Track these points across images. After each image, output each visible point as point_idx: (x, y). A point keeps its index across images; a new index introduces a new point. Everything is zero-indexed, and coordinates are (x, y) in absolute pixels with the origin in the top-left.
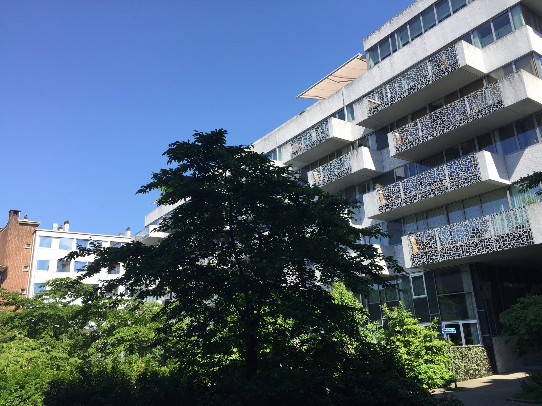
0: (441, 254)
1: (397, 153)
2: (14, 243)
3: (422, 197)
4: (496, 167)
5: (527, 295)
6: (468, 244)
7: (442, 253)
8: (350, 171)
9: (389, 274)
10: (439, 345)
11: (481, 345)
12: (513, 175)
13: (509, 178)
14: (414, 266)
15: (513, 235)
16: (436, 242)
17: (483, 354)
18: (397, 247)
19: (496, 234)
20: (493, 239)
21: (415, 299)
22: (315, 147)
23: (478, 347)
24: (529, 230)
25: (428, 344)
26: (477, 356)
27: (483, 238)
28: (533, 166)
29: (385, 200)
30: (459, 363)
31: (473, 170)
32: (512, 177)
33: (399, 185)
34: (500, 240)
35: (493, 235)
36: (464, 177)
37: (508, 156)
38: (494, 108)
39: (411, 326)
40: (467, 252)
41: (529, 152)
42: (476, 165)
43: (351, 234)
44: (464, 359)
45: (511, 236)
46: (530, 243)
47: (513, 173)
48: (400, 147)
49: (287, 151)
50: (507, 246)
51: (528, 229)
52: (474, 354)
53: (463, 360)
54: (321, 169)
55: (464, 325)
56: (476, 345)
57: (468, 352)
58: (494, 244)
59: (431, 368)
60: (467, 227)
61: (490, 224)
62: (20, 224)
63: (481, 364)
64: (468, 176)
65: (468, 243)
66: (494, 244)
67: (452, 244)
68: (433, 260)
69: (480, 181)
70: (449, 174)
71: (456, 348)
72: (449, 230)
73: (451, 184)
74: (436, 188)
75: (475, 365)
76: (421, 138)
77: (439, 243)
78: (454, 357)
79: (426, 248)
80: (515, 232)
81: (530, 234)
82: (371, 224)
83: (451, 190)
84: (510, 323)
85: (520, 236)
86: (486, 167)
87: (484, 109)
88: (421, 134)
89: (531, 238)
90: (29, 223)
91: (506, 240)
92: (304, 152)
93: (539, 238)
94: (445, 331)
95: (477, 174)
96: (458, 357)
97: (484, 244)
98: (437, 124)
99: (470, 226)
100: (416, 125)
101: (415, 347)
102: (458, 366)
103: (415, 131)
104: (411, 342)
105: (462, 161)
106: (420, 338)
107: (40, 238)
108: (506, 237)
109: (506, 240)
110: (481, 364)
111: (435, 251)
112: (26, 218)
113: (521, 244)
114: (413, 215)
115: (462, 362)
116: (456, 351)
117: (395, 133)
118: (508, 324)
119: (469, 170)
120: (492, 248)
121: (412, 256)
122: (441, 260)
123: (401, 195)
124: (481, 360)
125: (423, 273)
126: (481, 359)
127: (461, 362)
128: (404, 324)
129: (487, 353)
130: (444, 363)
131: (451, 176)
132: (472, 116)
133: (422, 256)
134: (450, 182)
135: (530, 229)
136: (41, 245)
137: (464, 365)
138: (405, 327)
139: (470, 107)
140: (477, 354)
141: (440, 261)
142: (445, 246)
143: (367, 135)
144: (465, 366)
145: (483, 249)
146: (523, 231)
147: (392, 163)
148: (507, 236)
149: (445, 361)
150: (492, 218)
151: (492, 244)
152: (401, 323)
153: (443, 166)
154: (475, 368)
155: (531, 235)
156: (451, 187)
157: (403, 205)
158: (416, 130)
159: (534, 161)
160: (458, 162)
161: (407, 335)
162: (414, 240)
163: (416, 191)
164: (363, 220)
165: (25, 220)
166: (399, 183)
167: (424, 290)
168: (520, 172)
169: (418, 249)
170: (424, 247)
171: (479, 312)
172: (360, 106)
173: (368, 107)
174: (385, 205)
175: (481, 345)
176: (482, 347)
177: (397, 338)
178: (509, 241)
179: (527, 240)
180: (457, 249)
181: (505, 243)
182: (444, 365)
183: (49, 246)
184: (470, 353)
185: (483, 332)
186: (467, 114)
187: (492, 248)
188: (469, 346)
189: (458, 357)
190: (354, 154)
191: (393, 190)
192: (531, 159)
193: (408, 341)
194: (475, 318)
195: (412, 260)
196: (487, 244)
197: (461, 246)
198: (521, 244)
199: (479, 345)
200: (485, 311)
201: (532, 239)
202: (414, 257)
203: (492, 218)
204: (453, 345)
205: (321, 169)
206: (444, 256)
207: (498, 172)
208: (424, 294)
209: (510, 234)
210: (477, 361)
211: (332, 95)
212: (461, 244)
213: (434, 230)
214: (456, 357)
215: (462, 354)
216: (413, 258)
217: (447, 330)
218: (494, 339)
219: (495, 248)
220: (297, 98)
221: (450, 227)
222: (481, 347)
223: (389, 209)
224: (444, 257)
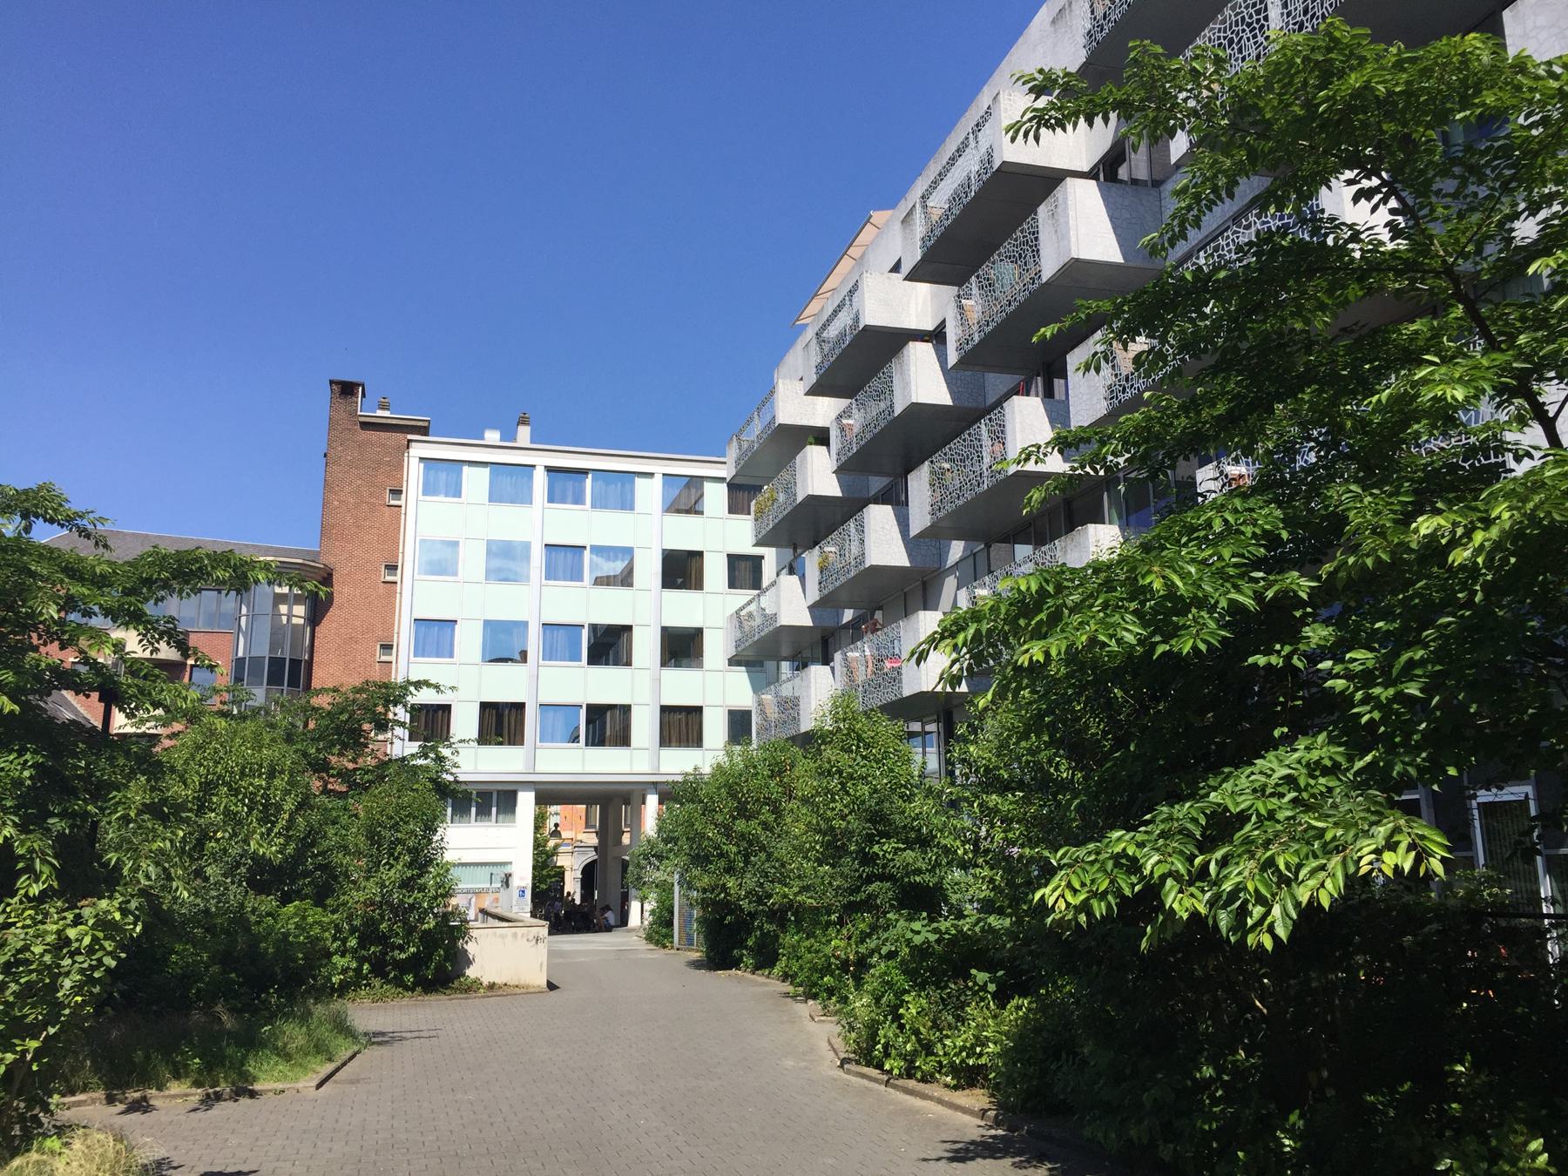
2: (348, 489)
9: (907, 564)
43: (1459, 165)
62: (366, 426)
90: (394, 422)
107: (422, 465)
112: (383, 407)
136: (429, 489)
165: (380, 413)
183: (627, 504)
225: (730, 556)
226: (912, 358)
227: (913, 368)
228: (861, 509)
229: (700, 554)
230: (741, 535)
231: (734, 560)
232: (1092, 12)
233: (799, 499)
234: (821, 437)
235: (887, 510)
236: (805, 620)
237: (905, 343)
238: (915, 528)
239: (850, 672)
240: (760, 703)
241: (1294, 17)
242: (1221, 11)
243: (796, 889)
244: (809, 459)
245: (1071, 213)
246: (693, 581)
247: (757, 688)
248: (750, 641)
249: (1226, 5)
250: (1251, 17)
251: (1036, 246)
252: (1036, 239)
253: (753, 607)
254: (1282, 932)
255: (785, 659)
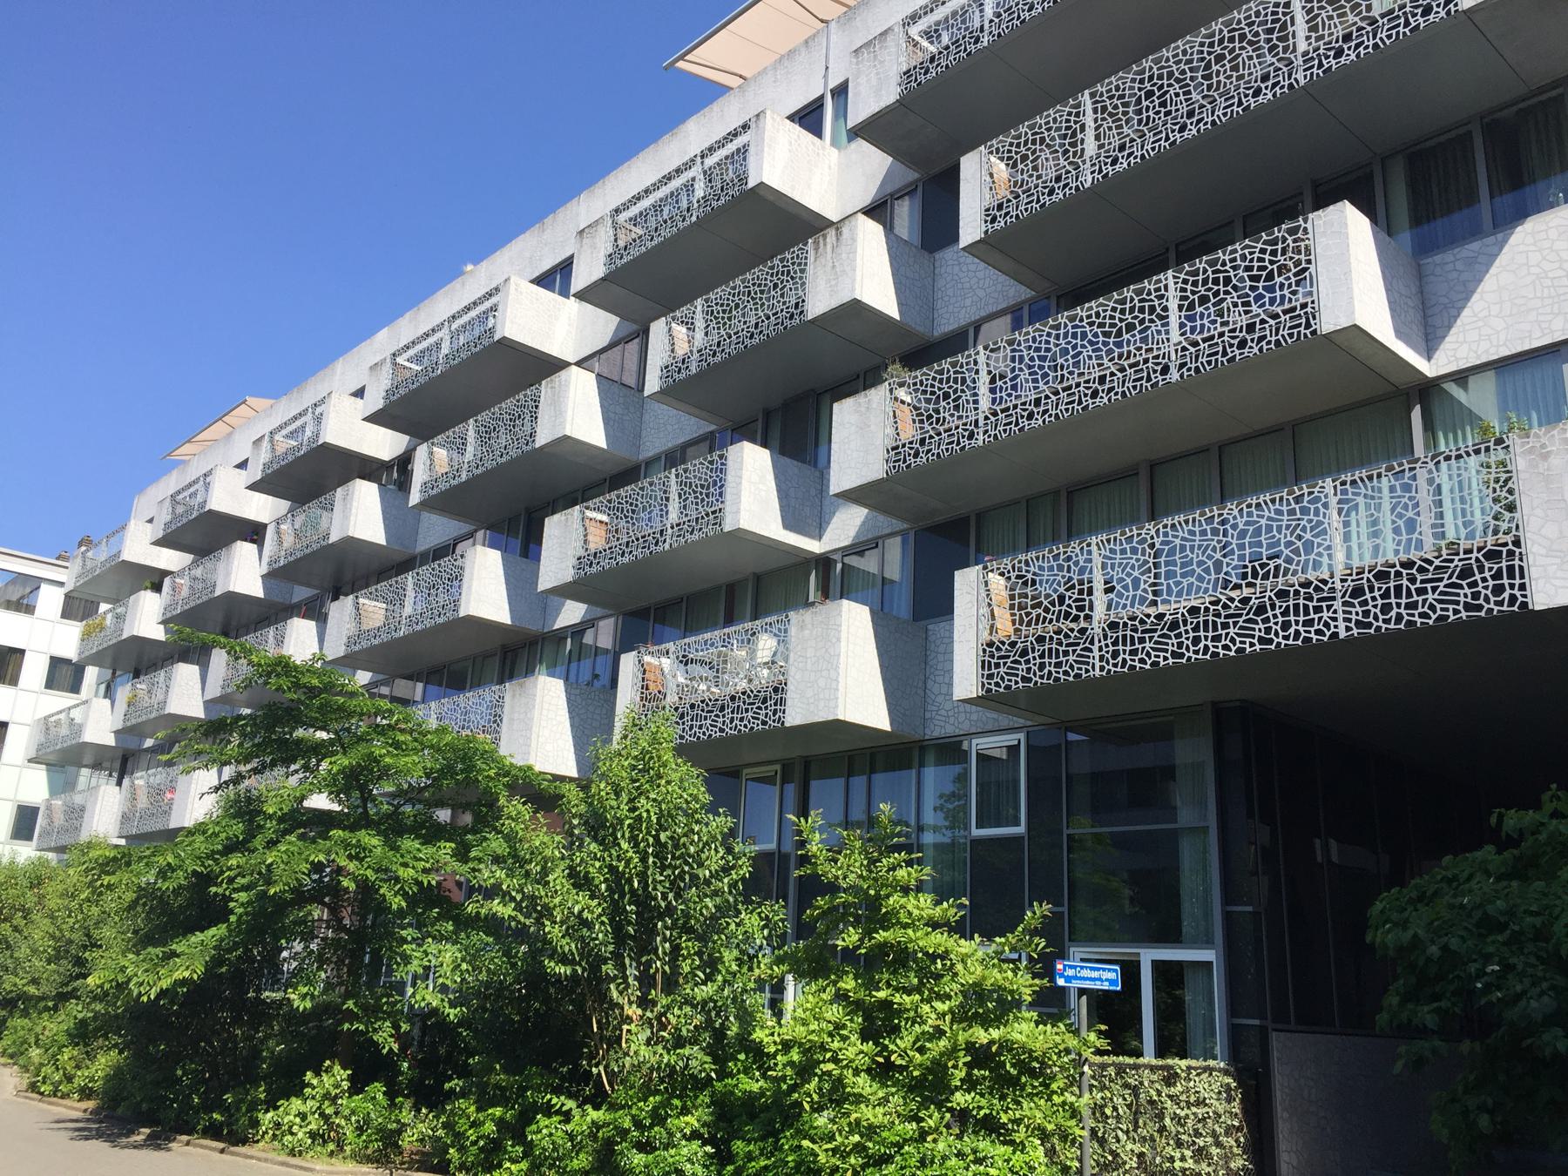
0: (1103, 643)
1: (986, 232)
3: (1060, 408)
4: (1387, 290)
5: (1545, 797)
6: (1225, 606)
7: (1109, 641)
8: (802, 312)
9: (509, 622)
10: (1039, 1046)
11: (1222, 1065)
12: (1447, 339)
13: (1428, 353)
14: (989, 690)
15: (1431, 569)
16: (1090, 592)
17: (1224, 1104)
18: (936, 628)
19: (1356, 563)
20: (1338, 585)
21: (977, 842)
22: (692, 225)
23: (1209, 1070)
24: (1510, 546)
25: (981, 1036)
26: (1200, 1111)
27: (1294, 580)
28: (1542, 298)
29: (914, 421)
30: (1118, 1141)
31: (1290, 286)
32: (1442, 347)
33: (976, 363)
34: (1371, 589)
35: (1341, 567)
36: (1244, 321)
37: (1438, 258)
38: (1414, 15)
39: (910, 932)
40: (1215, 639)
41: (1530, 240)
42: (1304, 265)
44: (1141, 1122)
45: (1422, 570)
46: (1512, 603)
47: (1450, 327)
48: (1000, 207)
49: (594, 247)
50: (1399, 618)
51: (1509, 539)
52: (1188, 1103)
53: (1136, 1127)
54: (699, 308)
55: (1158, 966)
56: (1201, 1063)
57: (1165, 1091)
58: (1337, 605)
59: (978, 1161)
60: (1230, 531)
61: (1335, 519)
63: (1214, 1151)
64: (1263, 316)
65: (1223, 598)
66: (1337, 605)
67: (1154, 603)
68: (1067, 669)
69: (1314, 332)
70: (1180, 307)
71: (1113, 1064)
72: (1152, 546)
73: (1184, 349)
74: (1122, 370)
75: (1188, 1153)
76: (1088, 164)
77: (1100, 600)
78: (1097, 1109)
79: (1045, 618)
80: (1444, 552)
81: (1517, 562)
82: (857, 536)
83: (1182, 376)
84: (1445, 948)
85: (1466, 573)
86: (1347, 273)
87: (1370, 25)
88: (1091, 147)
89: (1517, 582)
91: (1398, 588)
92: (649, 245)
93: (1557, 583)
94: (1070, 972)
95: (1304, 306)
96: (1115, 1109)
97: (1296, 606)
98: (1163, 105)
99: (1241, 526)
100: (1077, 115)
101: (917, 1040)
102: (1112, 1152)
103: (1073, 136)
104: (899, 1013)
105: (1246, 251)
106: (949, 997)
108: (1398, 574)
109: (1398, 588)
110: (1214, 1151)
111: (1083, 631)
113: (1468, 607)
114: (1016, 502)
115: (1132, 1134)
116: (1111, 1081)
117: (993, 159)
118: (1434, 950)
119: (1271, 289)
120: (1327, 625)
121: (984, 651)
122: (1102, 668)
123: (976, 402)
124: (1214, 1134)
125: (1022, 736)
126: (1216, 1127)
127: (1127, 1132)
128: (886, 922)
129: (1242, 1101)
130: (1044, 1136)
131: (1191, 318)
132: (1312, 59)
133: (1024, 653)
134: (1184, 344)
135: (1517, 543)
137: (1137, 1148)
138: (881, 936)
139: (1307, 22)
140: (1201, 1103)
141: (1097, 673)
142: (1124, 613)
143: (891, 195)
144: (1141, 1155)
145: (1286, 626)
146: (1479, 550)
147: (968, 302)
148: (1404, 572)
149: (1050, 1127)
150: (1344, 492)
151: (1329, 607)
152: (873, 914)
153: (1161, 276)
154: (1187, 1166)
155: (1521, 568)
156: (1186, 364)
157: (980, 439)
158: (1074, 134)
159: (1550, 275)
160: (1227, 258)
161: (886, 976)
162: (1005, 594)
163: (1041, 384)
164: (831, 519)
166: (978, 353)
167: (1017, 808)
168: (1481, 324)
169: (1014, 622)
170: (1038, 616)
171: (1228, 917)
172: (875, 56)
173: (902, 59)
174: (911, 443)
175: (1222, 1065)
176: (1226, 1072)
177: (841, 985)
178: (1409, 595)
179: (1498, 590)
180: (1174, 625)
181: (1393, 601)
182: (1041, 1151)
184: (1169, 1096)
185: (1234, 1007)
186: (1294, 51)
187: (1327, 625)
188: (1170, 1062)
189: (1115, 1109)
190: (825, 245)
191: (948, 382)
192: (1533, 270)
193: (886, 1004)
194: (1207, 943)
195: (983, 668)
196: (1306, 607)
197: (1194, 611)
198: (1468, 607)
199: (1211, 1063)
200: (1253, 913)
201: (1522, 587)
202: (993, 654)
203: (1344, 492)
204: (1099, 1052)
205: (699, 308)
206: (1115, 654)
207: (1391, 309)
208: (1018, 824)
209: (1419, 563)
210: (1197, 1134)
211: (791, 53)
212: (1195, 603)
213: (1089, 545)
214: (1108, 1111)
215: (1136, 1096)
216: (987, 658)
217: (1086, 973)
218: (1277, 1041)
219: (1342, 625)
220: (666, 68)
221: (1157, 531)
222: (1220, 1070)
223: (924, 460)
224: (1114, 658)
225: (52, 658)
226: (237, 554)
227: (236, 563)
228: (285, 619)
229: (22, 652)
230: (67, 640)
231: (56, 663)
232: (616, 240)
233: (125, 636)
234: (254, 532)
235: (311, 625)
236: (110, 740)
237: (345, 480)
238: (208, 696)
239: (134, 798)
240: (49, 808)
241: (1108, 151)
242: (733, 279)
243: (25, 981)
244: (141, 602)
245: (355, 504)
246: (8, 677)
247: (54, 791)
248: (52, 749)
249: (1023, 122)
250: (1116, 107)
251: (801, 278)
252: (537, 407)
253: (62, 716)
254: (152, 997)
255: (86, 766)
